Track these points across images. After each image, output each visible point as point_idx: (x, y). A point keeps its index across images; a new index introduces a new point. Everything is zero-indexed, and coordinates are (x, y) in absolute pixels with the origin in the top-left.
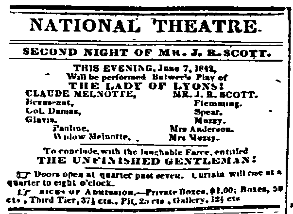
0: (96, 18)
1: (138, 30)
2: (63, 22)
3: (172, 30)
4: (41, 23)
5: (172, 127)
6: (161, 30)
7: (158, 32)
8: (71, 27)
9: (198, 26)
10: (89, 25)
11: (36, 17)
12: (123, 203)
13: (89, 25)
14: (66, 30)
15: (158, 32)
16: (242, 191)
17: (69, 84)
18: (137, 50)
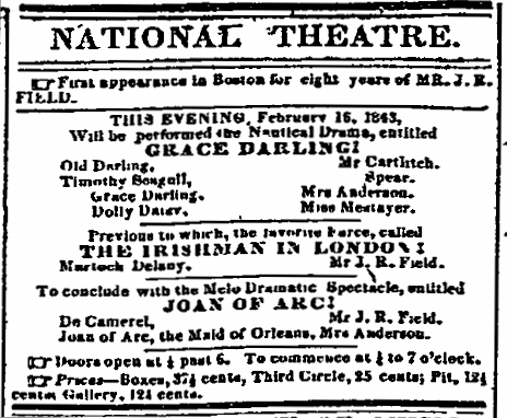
0: (165, 26)
1: (238, 43)
2: (108, 32)
3: (303, 43)
5: (304, 188)
6: (285, 43)
7: (279, 46)
8: (123, 40)
9: (351, 36)
10: (153, 38)
11: (62, 25)
12: (401, 322)
13: (153, 38)
14: (113, 45)
15: (279, 46)
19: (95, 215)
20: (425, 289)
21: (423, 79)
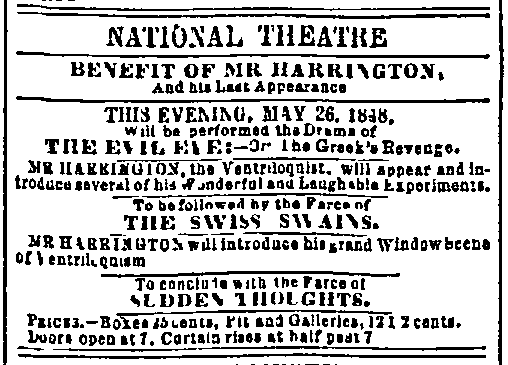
4: (110, 37)
16: (379, 173)
17: (236, 295)
18: (188, 67)
19: (74, 74)
20: (237, 245)
21: (49, 242)
